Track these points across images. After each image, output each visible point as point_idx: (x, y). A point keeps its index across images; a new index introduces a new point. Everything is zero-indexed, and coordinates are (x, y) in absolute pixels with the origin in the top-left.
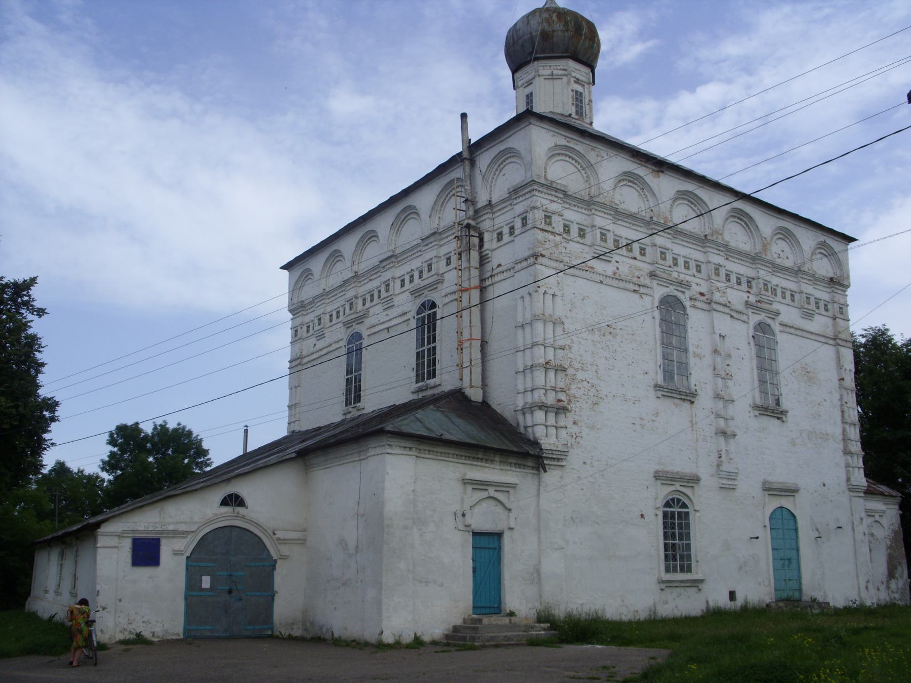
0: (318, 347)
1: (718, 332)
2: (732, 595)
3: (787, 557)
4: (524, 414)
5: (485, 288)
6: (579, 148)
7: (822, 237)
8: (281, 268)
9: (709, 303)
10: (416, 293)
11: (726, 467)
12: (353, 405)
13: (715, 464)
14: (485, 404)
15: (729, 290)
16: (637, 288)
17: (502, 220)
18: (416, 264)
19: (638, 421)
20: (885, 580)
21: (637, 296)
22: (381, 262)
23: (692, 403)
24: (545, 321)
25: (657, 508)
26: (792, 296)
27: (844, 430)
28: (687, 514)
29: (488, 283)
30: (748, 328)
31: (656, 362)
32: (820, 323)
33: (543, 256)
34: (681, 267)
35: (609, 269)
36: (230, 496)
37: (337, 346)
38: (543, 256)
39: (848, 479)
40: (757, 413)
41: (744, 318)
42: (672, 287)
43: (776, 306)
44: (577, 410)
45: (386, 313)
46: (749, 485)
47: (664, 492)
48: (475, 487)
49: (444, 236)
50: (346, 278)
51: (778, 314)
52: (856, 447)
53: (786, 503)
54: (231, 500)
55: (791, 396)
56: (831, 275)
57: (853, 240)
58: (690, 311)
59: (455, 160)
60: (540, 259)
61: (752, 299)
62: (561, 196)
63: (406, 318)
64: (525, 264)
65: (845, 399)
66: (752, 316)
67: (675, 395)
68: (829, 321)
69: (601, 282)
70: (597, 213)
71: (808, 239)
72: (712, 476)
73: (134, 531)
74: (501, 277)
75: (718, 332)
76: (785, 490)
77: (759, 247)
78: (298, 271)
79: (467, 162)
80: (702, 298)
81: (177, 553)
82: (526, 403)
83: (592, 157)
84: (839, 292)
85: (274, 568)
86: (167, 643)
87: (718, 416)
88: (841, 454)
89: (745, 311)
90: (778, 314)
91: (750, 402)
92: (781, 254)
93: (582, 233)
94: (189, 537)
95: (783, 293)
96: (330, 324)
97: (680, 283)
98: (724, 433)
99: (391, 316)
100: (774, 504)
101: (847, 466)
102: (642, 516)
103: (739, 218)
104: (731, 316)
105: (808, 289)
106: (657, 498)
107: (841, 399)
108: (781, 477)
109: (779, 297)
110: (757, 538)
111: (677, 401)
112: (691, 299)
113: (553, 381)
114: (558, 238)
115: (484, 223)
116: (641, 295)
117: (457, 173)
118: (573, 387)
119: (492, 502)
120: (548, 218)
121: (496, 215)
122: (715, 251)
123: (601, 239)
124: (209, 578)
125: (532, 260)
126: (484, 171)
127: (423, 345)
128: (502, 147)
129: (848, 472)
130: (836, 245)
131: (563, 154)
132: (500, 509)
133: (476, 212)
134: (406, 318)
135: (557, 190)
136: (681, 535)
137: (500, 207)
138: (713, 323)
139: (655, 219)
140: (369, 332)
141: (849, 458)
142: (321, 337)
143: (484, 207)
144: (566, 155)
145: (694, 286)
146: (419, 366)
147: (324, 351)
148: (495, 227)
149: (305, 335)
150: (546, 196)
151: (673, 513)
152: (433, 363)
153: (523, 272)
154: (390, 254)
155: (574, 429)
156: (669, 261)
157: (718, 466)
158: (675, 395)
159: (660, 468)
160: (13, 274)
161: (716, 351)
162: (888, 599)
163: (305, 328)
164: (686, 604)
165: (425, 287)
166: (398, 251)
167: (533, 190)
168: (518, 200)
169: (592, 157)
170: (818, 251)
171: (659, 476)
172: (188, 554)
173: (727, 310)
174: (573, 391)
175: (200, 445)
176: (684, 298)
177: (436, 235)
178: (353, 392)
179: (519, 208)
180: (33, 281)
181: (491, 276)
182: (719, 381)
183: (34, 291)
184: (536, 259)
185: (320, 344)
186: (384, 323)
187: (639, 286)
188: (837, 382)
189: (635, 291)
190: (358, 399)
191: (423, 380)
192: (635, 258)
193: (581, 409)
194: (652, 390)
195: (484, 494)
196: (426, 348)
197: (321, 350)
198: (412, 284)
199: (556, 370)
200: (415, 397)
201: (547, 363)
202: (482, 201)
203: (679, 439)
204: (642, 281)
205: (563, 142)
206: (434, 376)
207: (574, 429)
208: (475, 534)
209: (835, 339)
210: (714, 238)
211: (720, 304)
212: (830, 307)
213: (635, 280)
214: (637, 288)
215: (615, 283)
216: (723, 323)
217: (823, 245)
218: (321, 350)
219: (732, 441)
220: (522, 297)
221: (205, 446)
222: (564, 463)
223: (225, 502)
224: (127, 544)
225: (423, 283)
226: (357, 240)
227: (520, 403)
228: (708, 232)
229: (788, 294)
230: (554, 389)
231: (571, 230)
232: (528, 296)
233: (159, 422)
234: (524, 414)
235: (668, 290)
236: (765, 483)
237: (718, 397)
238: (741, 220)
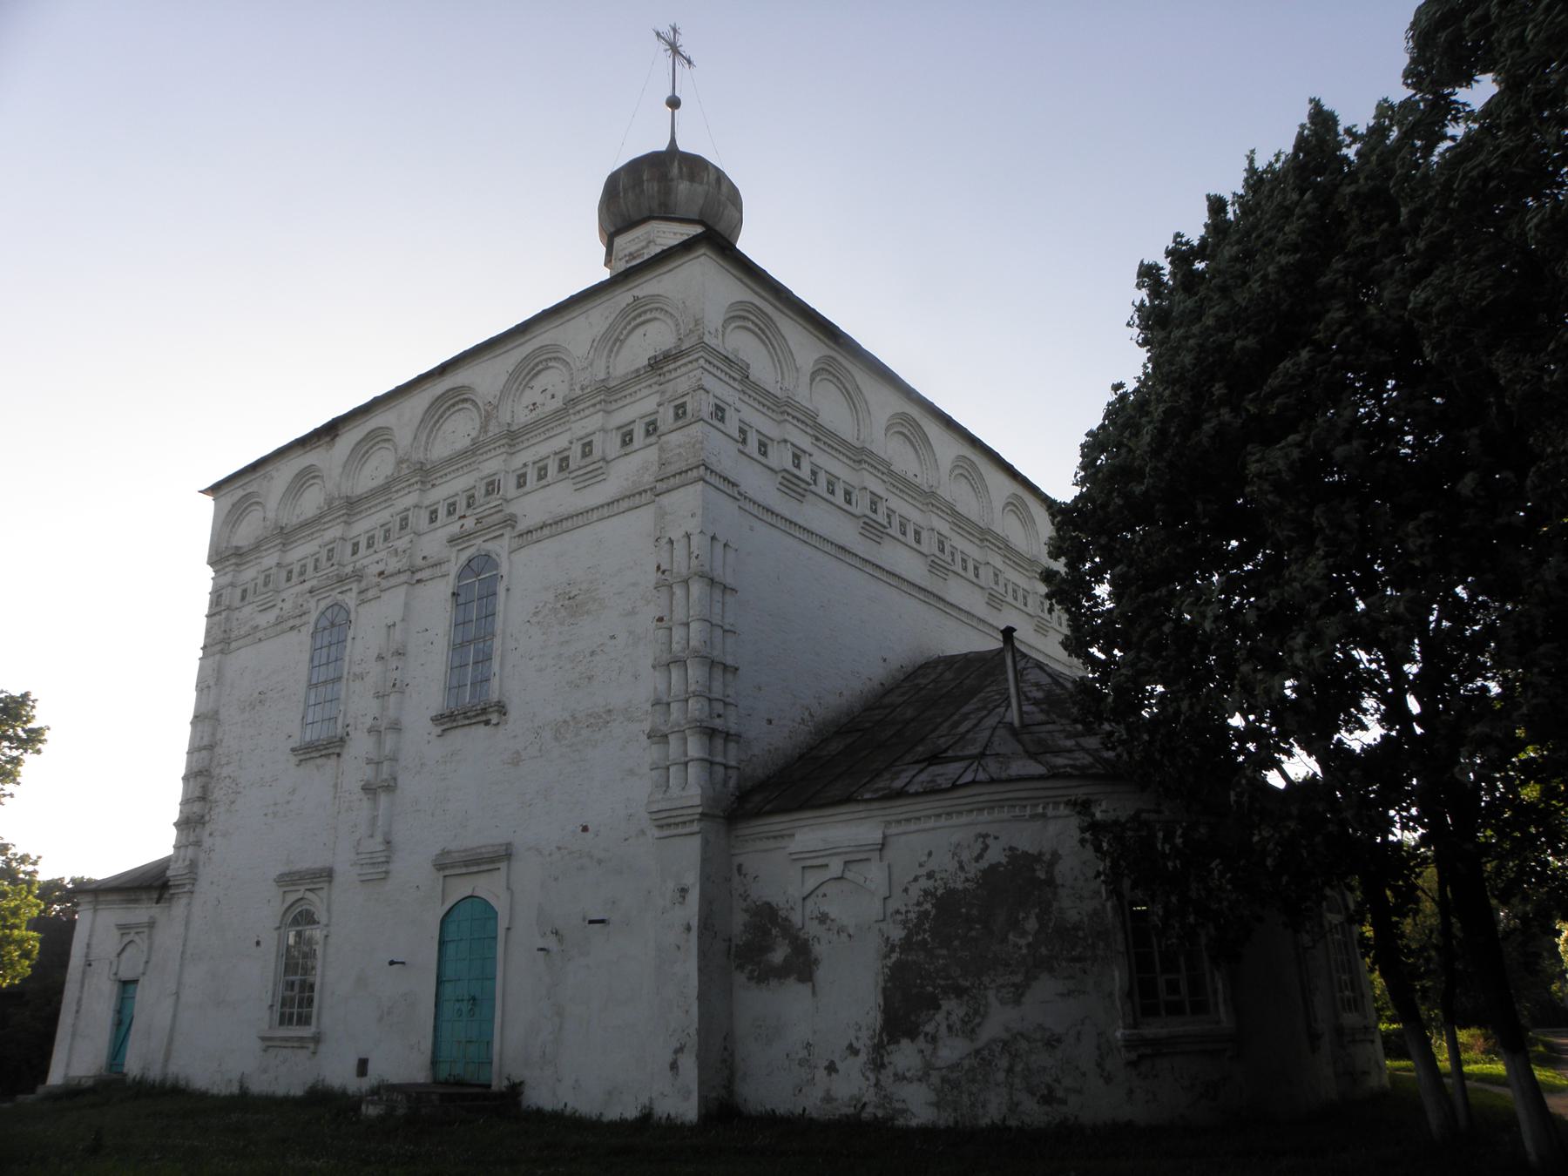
2: (362, 1067)
3: (297, 1000)
20: (864, 1042)
47: (34, 857)
55: (525, 671)
76: (476, 862)
86: (692, 1129)
102: (258, 943)
111: (319, 761)
120: (719, 412)
128: (769, 309)
162: (870, 1096)
164: (286, 1076)
205: (241, 493)
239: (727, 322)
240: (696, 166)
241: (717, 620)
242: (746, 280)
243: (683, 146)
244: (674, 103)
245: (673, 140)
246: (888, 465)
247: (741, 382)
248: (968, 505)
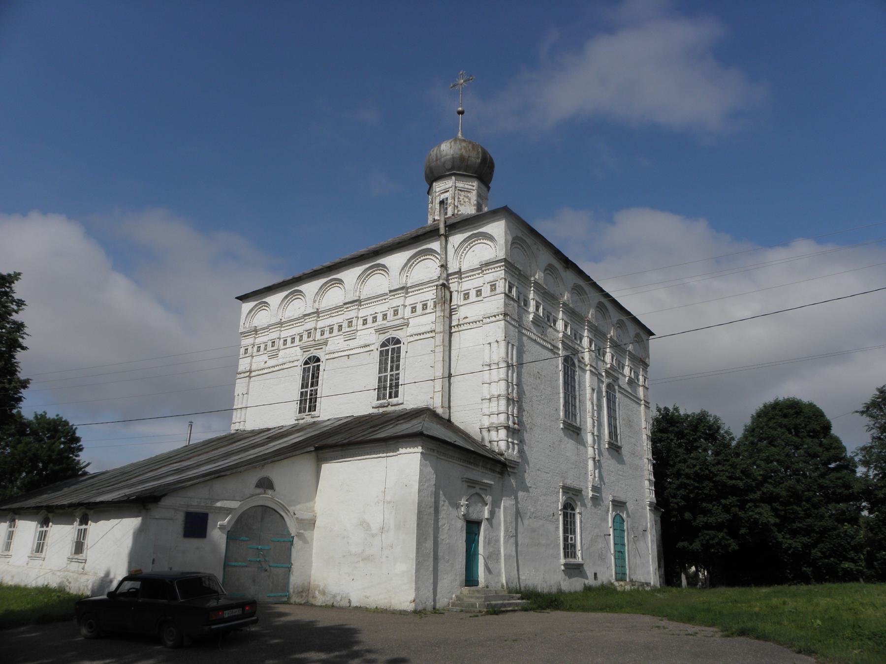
0: (267, 365)
4: (489, 431)
7: (638, 330)
8: (237, 298)
10: (380, 331)
12: (307, 413)
14: (449, 421)
17: (469, 284)
22: (345, 304)
57: (653, 334)
58: (577, 369)
64: (493, 319)
71: (632, 329)
73: (188, 506)
79: (443, 238)
85: (292, 543)
96: (282, 347)
99: (352, 346)
126: (456, 247)
130: (643, 335)
133: (448, 275)
140: (328, 357)
143: (455, 273)
154: (356, 298)
160: (6, 270)
163: (255, 348)
175: (74, 433)
178: (308, 401)
180: (16, 276)
181: (457, 325)
183: (16, 286)
190: (312, 408)
191: (384, 398)
196: (389, 373)
198: (376, 324)
200: (376, 411)
202: (453, 267)
205: (520, 235)
206: (396, 396)
220: (490, 344)
221: (78, 434)
222: (516, 471)
224: (180, 518)
233: (40, 412)
234: (489, 431)
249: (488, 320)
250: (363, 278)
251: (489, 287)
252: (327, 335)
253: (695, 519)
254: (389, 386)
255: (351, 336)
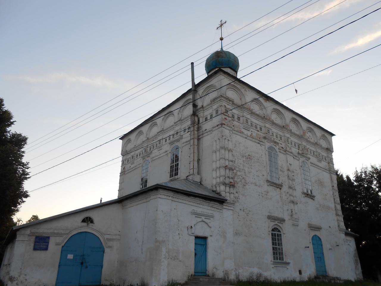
1: (289, 163)
3: (319, 258)
5: (200, 139)
6: (238, 86)
7: (323, 133)
9: (285, 152)
11: (295, 216)
13: (290, 214)
15: (292, 148)
16: (259, 142)
17: (207, 113)
18: (172, 133)
19: (260, 194)
21: (259, 145)
22: (158, 133)
23: (281, 189)
24: (225, 149)
25: (269, 231)
26: (314, 153)
27: (335, 206)
28: (280, 235)
29: (201, 137)
30: (299, 163)
31: (267, 171)
32: (323, 164)
33: (224, 124)
34: (275, 137)
35: (249, 133)
36: (87, 218)
37: (139, 166)
38: (224, 124)
39: (339, 226)
40: (304, 196)
41: (298, 159)
42: (272, 144)
43: (308, 156)
44: (238, 187)
45: (159, 152)
46: (303, 225)
47: (272, 224)
48: (197, 216)
49: (183, 121)
50: (144, 140)
51: (309, 159)
52: (340, 213)
53: (317, 233)
54: (87, 220)
56: (326, 147)
59: (189, 91)
60: (223, 126)
61: (300, 152)
62: (231, 103)
63: (167, 153)
65: (335, 194)
66: (300, 158)
67: (274, 185)
68: (327, 164)
69: (246, 138)
70: (244, 112)
71: (319, 133)
72: (289, 219)
74: (206, 134)
75: (289, 163)
77: (302, 133)
78: (126, 140)
80: (282, 149)
81: (57, 244)
82: (217, 183)
83: (243, 90)
84: (330, 154)
87: (291, 195)
88: (335, 215)
89: (298, 156)
90: (309, 159)
91: (302, 191)
92: (309, 137)
93: (239, 118)
94: (65, 236)
95: (310, 151)
97: (275, 142)
98: (293, 202)
100: (313, 233)
101: (338, 220)
103: (294, 122)
104: (293, 158)
105: (319, 151)
106: (269, 227)
107: (333, 194)
108: (316, 222)
109: (309, 153)
110: (308, 247)
112: (279, 149)
113: (228, 174)
114: (230, 119)
115: (200, 114)
116: (261, 145)
117: (190, 97)
118: (236, 178)
119: (203, 223)
121: (205, 111)
122: (286, 132)
123: (246, 122)
124: (68, 255)
125: (220, 126)
127: (173, 163)
128: (208, 85)
129: (338, 223)
131: (232, 88)
132: (206, 226)
134: (167, 153)
135: (230, 101)
136: (278, 243)
137: (206, 108)
138: (287, 159)
139: (266, 117)
141: (338, 217)
142: (133, 163)
144: (233, 89)
145: (280, 145)
146: (171, 171)
147: (134, 169)
148: (204, 116)
149: (127, 163)
150: (226, 102)
151: (275, 234)
152: (177, 169)
153: (216, 131)
154: (162, 130)
155: (236, 195)
156: (271, 134)
157: (292, 216)
158: (274, 185)
159: (270, 214)
161: (288, 170)
163: (127, 161)
165: (174, 141)
166: (165, 129)
167: (221, 99)
168: (214, 104)
169: (243, 90)
170: (322, 138)
171: (269, 217)
172: (63, 244)
173: (292, 155)
174: (236, 179)
176: (277, 148)
177: (180, 121)
179: (215, 107)
181: (202, 134)
182: (290, 181)
184: (222, 125)
185: (132, 166)
186: (158, 156)
187: (260, 141)
188: (331, 187)
189: (258, 143)
192: (258, 131)
193: (239, 185)
194: (265, 182)
195: (200, 220)
196: (174, 164)
197: (132, 168)
199: (230, 170)
201: (226, 167)
203: (275, 203)
204: (261, 140)
206: (177, 174)
207: (236, 195)
208: (197, 237)
209: (329, 171)
210: (287, 127)
211: (289, 152)
212: (327, 159)
213: (258, 139)
214: (259, 142)
215: (251, 139)
216: (290, 159)
217: (323, 136)
218: (132, 168)
219: (296, 206)
220: (216, 141)
223: (84, 221)
225: (174, 139)
226: (149, 126)
227: (214, 183)
228: (284, 125)
229: (312, 152)
230: (229, 177)
231: (235, 117)
232: (218, 140)
235: (270, 144)
236: (309, 224)
237: (290, 187)
238: (295, 122)
239: (290, 122)
240: (228, 54)
241: (306, 185)
242: (306, 121)
243: (225, 49)
244: (222, 39)
245: (222, 48)
246: (291, 130)
247: (307, 142)
248: (278, 121)
249: (215, 129)
250: (165, 120)
251: (215, 111)
252: (152, 149)
253: (30, 231)
254: (174, 170)
255: (160, 148)
